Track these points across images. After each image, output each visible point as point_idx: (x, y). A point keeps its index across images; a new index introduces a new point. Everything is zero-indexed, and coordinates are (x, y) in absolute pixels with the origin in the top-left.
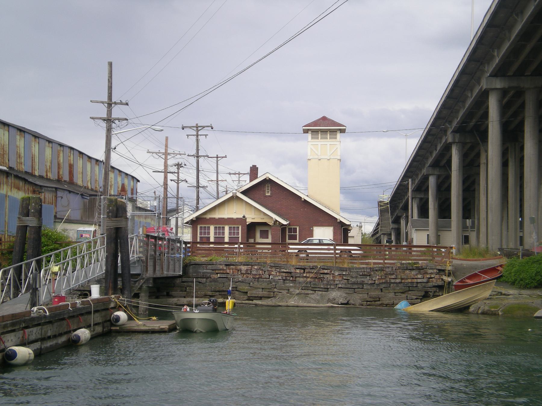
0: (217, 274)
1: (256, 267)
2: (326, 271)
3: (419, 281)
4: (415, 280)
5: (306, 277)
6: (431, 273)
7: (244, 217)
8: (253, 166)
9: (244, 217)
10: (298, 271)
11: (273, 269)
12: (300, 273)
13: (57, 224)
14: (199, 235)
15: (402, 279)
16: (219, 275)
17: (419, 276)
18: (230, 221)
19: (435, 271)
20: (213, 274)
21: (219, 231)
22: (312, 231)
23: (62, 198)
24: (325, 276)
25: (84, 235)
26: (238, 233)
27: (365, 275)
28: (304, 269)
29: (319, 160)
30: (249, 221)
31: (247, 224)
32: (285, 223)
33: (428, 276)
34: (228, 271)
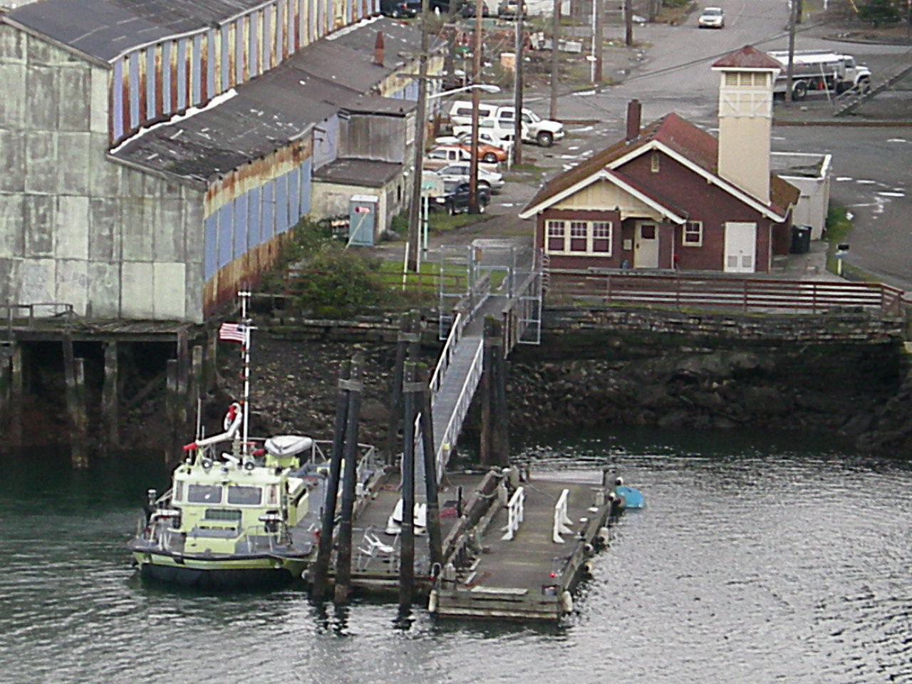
0: (580, 323)
1: (633, 315)
2: (730, 323)
3: (857, 337)
4: (852, 337)
5: (702, 330)
6: (875, 327)
7: (617, 209)
8: (635, 101)
9: (617, 209)
10: (691, 321)
11: (657, 318)
12: (694, 324)
13: (315, 184)
14: (547, 235)
15: (834, 335)
16: (582, 325)
17: (858, 331)
18: (595, 215)
19: (880, 324)
20: (574, 323)
21: (579, 230)
22: (724, 228)
23: (321, 140)
24: (729, 329)
25: (361, 209)
26: (607, 234)
27: (783, 329)
28: (700, 319)
29: (737, 118)
30: (623, 216)
31: (622, 219)
32: (680, 221)
33: (870, 331)
34: (594, 319)
